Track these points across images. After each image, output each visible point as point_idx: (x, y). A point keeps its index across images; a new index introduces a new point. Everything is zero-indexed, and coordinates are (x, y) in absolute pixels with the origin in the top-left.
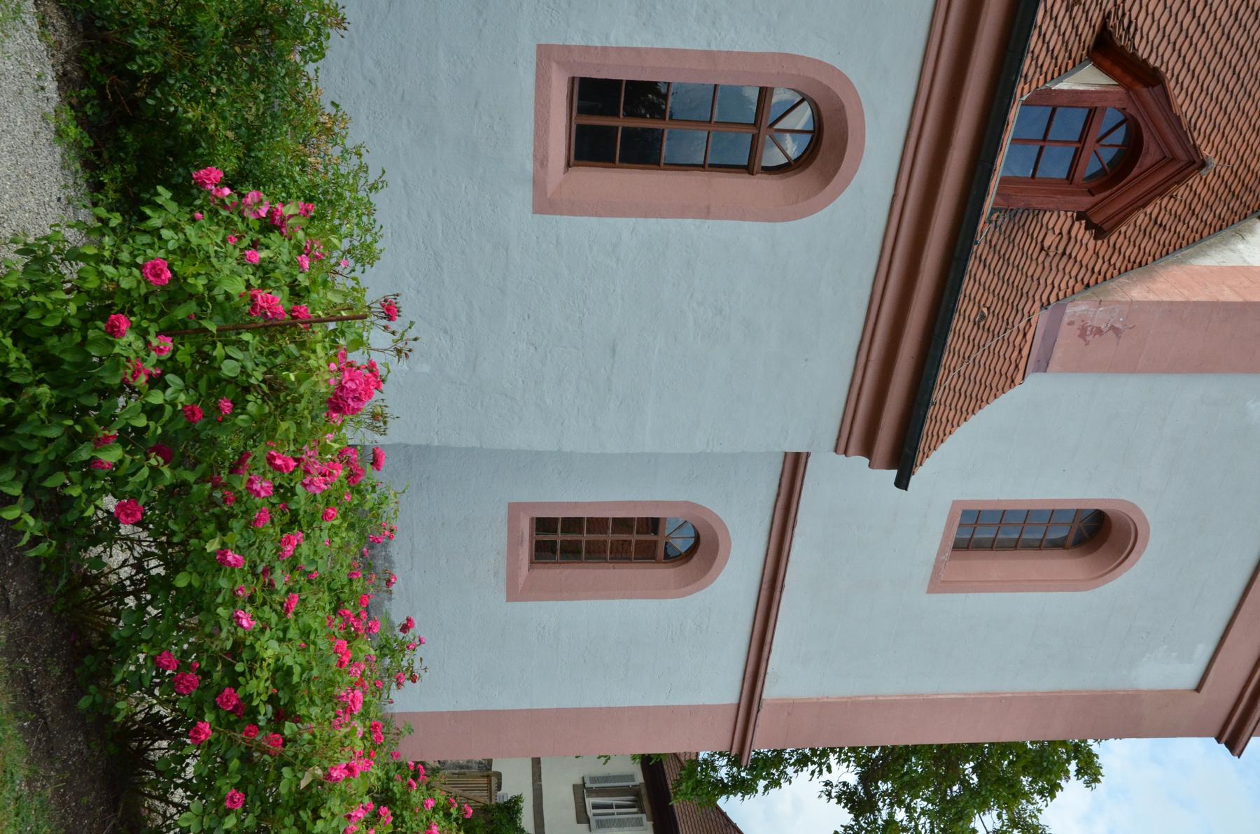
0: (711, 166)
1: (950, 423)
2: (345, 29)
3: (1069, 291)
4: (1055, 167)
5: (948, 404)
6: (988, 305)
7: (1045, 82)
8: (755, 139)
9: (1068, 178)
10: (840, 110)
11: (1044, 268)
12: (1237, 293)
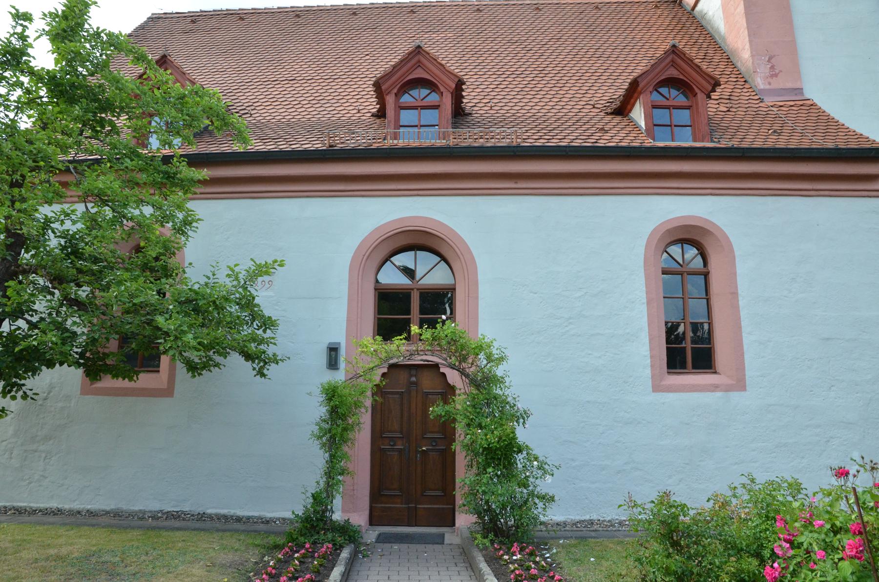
0: (707, 295)
1: (847, 134)
2: (670, 492)
3: (750, 90)
4: (683, 116)
5: (834, 138)
6: (767, 131)
7: (642, 133)
8: (690, 273)
9: (689, 109)
10: (669, 232)
11: (739, 107)
12: (738, 5)
